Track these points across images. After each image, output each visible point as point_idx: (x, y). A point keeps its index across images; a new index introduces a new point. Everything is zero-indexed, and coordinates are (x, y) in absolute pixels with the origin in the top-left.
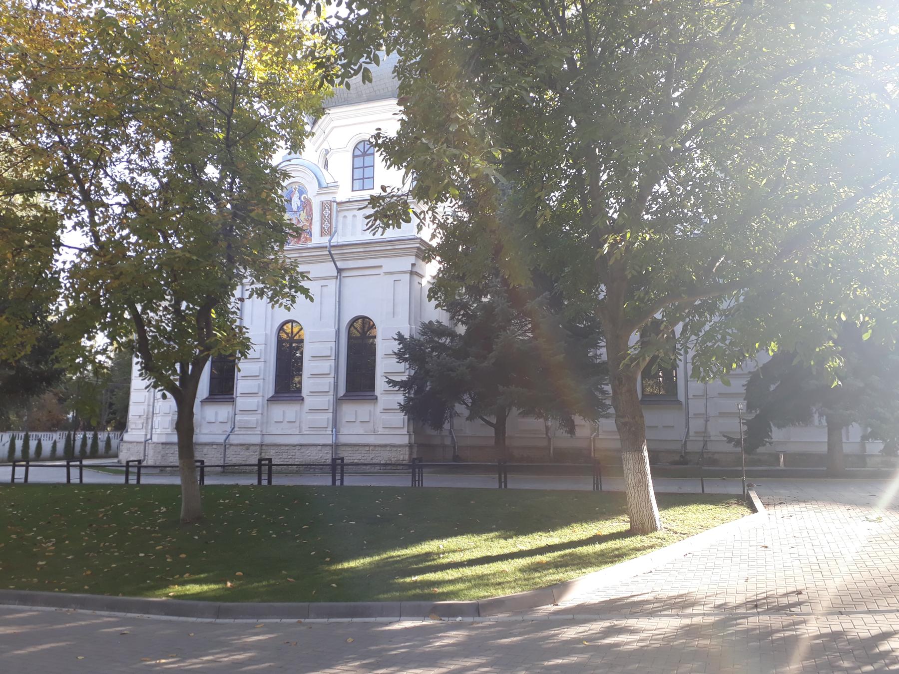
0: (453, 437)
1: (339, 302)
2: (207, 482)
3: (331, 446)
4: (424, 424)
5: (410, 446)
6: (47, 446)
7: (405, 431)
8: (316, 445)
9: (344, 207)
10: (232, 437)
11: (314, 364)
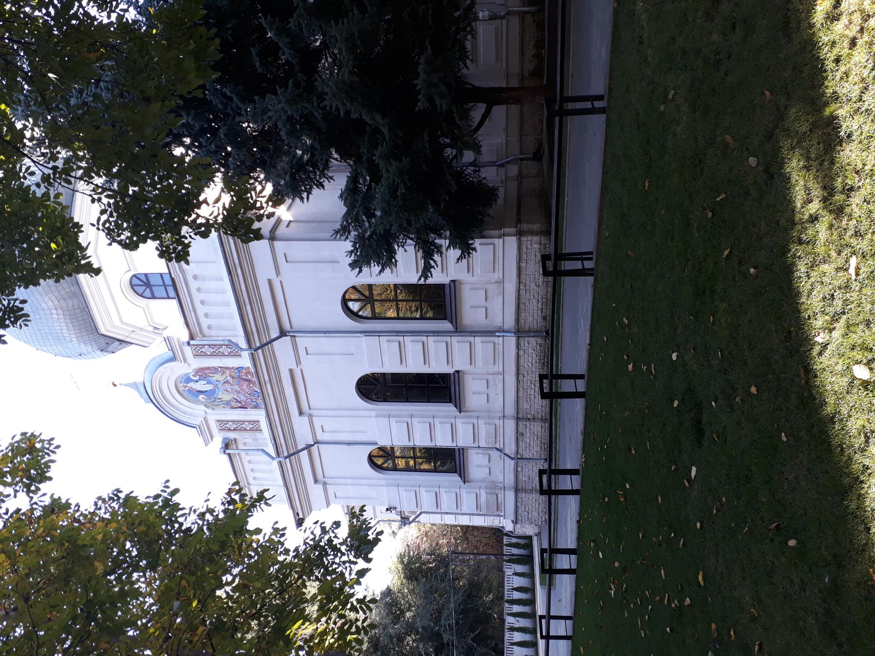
0: (507, 162)
1: (325, 332)
3: (518, 338)
4: (488, 215)
5: (520, 234)
6: (518, 582)
7: (498, 242)
8: (518, 357)
9: (195, 329)
11: (410, 361)
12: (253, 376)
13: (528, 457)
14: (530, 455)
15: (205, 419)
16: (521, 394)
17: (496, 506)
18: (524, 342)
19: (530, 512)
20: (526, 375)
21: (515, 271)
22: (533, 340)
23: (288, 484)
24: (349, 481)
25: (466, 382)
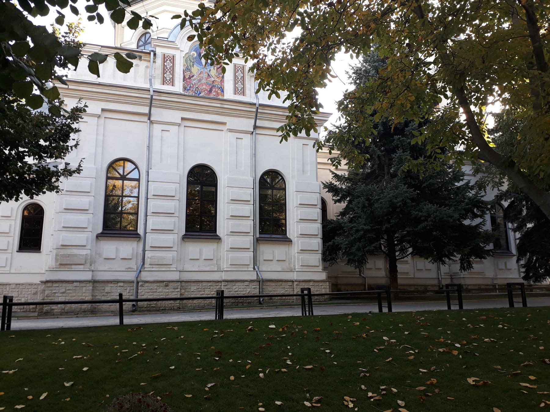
2: (15, 325)
7: (320, 269)
12: (214, 96)
13: (139, 291)
14: (143, 293)
15: (178, 49)
16: (204, 284)
17: (69, 263)
19: (64, 295)
20: (226, 287)
21: (231, 279)
23: (100, 87)
24: (101, 138)
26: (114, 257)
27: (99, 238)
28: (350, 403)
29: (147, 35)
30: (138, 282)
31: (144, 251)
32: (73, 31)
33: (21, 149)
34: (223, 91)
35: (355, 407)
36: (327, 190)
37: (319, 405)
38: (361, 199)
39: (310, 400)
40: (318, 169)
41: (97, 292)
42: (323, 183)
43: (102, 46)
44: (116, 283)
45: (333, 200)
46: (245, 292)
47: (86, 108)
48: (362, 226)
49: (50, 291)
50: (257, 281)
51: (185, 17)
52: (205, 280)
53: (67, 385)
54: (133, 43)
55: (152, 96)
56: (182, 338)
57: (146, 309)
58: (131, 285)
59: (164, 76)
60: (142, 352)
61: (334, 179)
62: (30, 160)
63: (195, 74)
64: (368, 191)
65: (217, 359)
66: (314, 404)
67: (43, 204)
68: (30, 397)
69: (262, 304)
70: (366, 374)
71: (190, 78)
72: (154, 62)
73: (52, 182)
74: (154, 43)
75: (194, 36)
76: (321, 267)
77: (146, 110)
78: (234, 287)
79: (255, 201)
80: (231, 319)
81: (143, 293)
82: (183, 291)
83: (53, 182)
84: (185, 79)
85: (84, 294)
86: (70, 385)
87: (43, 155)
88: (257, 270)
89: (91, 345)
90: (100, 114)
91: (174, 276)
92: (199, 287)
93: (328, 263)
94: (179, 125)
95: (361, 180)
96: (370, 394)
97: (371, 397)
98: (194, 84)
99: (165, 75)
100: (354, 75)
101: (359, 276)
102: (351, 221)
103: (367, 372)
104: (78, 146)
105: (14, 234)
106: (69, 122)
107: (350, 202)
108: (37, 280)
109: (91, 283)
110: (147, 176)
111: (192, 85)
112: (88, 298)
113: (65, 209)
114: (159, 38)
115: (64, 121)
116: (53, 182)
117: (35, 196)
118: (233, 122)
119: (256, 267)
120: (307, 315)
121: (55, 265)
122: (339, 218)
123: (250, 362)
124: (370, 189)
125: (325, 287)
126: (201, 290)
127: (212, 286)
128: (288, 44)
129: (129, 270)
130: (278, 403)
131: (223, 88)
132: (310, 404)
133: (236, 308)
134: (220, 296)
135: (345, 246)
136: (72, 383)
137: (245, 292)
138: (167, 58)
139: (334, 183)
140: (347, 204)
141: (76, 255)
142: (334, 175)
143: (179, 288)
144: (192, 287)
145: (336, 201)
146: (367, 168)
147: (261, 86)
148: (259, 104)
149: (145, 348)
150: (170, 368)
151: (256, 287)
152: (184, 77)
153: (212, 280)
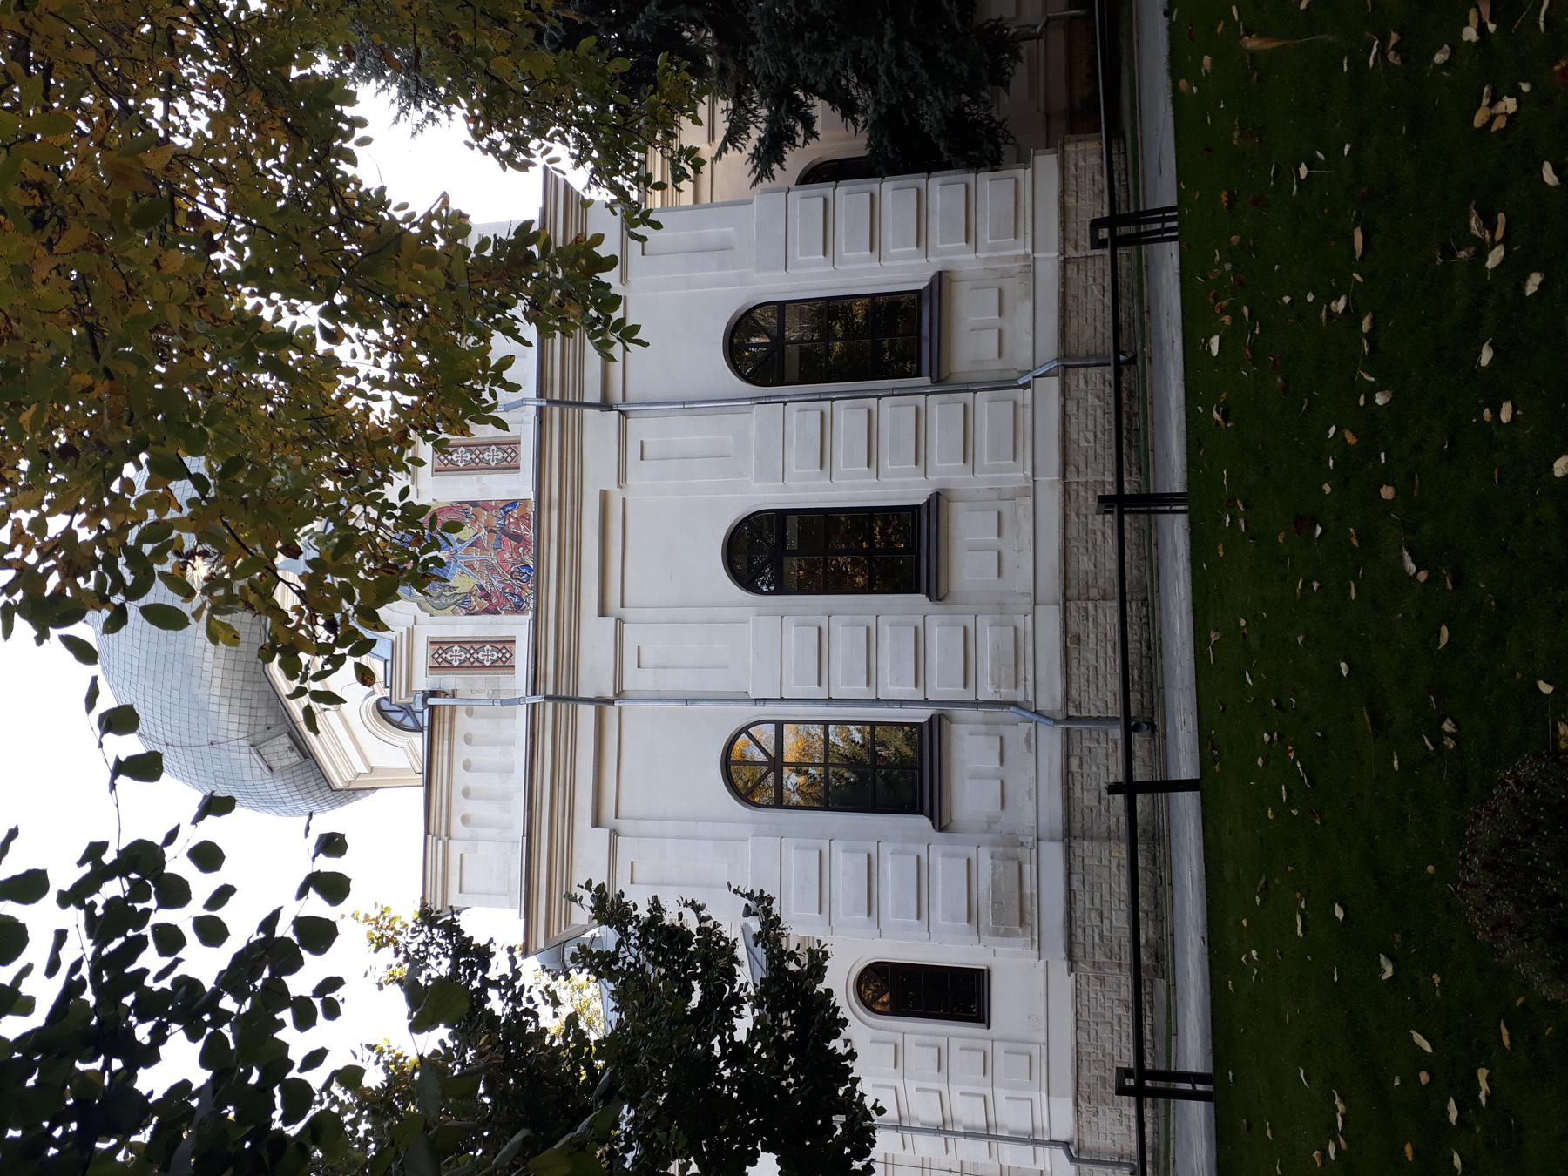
7: (1024, 175)
10: (1044, 704)
13: (1094, 714)
14: (1099, 703)
15: (410, 632)
16: (1073, 532)
17: (1016, 902)
18: (1077, 379)
19: (1106, 914)
20: (1082, 468)
22: (1095, 374)
25: (954, 740)
26: (999, 782)
27: (944, 824)
28: (1500, 107)
29: (384, 708)
30: (1069, 718)
31: (977, 704)
32: (390, 933)
33: (717, 1052)
34: (513, 503)
35: (1515, 92)
36: (775, 166)
37: (1501, 218)
38: (798, 55)
39: (1482, 250)
40: (714, 201)
41: (1099, 828)
42: (755, 183)
43: (427, 831)
44: (1070, 776)
45: (805, 142)
46: (1098, 409)
47: (594, 886)
48: (886, 46)
49: (1097, 948)
50: (1065, 374)
51: (307, 695)
52: (1062, 531)
53: (1389, 971)
54: (411, 745)
55: (547, 698)
56: (1247, 623)
57: (1146, 694)
58: (1075, 736)
59: (489, 666)
60: (1290, 748)
61: (740, 146)
62: (743, 1026)
63: (476, 581)
64: (772, 33)
65: (1319, 530)
66: (1499, 235)
67: (856, 966)
68: (1424, 1077)
69: (1135, 356)
70: (1392, 42)
71: (487, 596)
72: (454, 695)
73: (798, 971)
74: (403, 696)
75: (358, 667)
76: (1020, 173)
77: (587, 713)
78: (1083, 443)
79: (823, 397)
80: (1188, 471)
81: (1099, 703)
82: (1093, 593)
83: (798, 968)
84: (492, 608)
85: (1105, 862)
86: (1389, 962)
87: (727, 994)
88: (1031, 378)
89: (1263, 881)
90: (607, 831)
91: (1050, 619)
92: (1081, 550)
93: (1004, 148)
94: (620, 621)
95: (739, 59)
96: (1470, 34)
97: (1482, 29)
98: (501, 585)
99: (487, 664)
100: (424, 105)
101: (1042, 41)
102: (868, 80)
103: (1384, 41)
104: (698, 903)
105: (941, 1035)
106: (635, 928)
107: (810, 89)
108: (1063, 981)
109: (1072, 845)
110: (767, 703)
111: (507, 590)
112: (1121, 852)
113: (869, 913)
114: (388, 684)
115: (632, 941)
116: (798, 968)
117: (840, 1016)
118: (598, 470)
119: (1021, 382)
120: (1175, 224)
121: (1024, 936)
122: (861, 119)
123: (1333, 429)
124: (764, 30)
125: (1080, 155)
126: (1089, 541)
127: (1078, 510)
128: (353, 342)
129: (1033, 744)
130: (1486, 356)
131: (504, 504)
132: (1497, 249)
133: (1146, 437)
134: (1115, 503)
135: (951, 98)
136: (1383, 958)
137: (1098, 409)
138: (440, 660)
139: (755, 148)
140: (816, 98)
141: (995, 886)
142: (728, 145)
143: (1084, 605)
144: (1081, 568)
145: (811, 134)
146: (702, 41)
147: (484, 415)
148: (538, 397)
149: (1275, 735)
150: (1345, 674)
151: (1081, 377)
152: (487, 611)
153: (1062, 512)
